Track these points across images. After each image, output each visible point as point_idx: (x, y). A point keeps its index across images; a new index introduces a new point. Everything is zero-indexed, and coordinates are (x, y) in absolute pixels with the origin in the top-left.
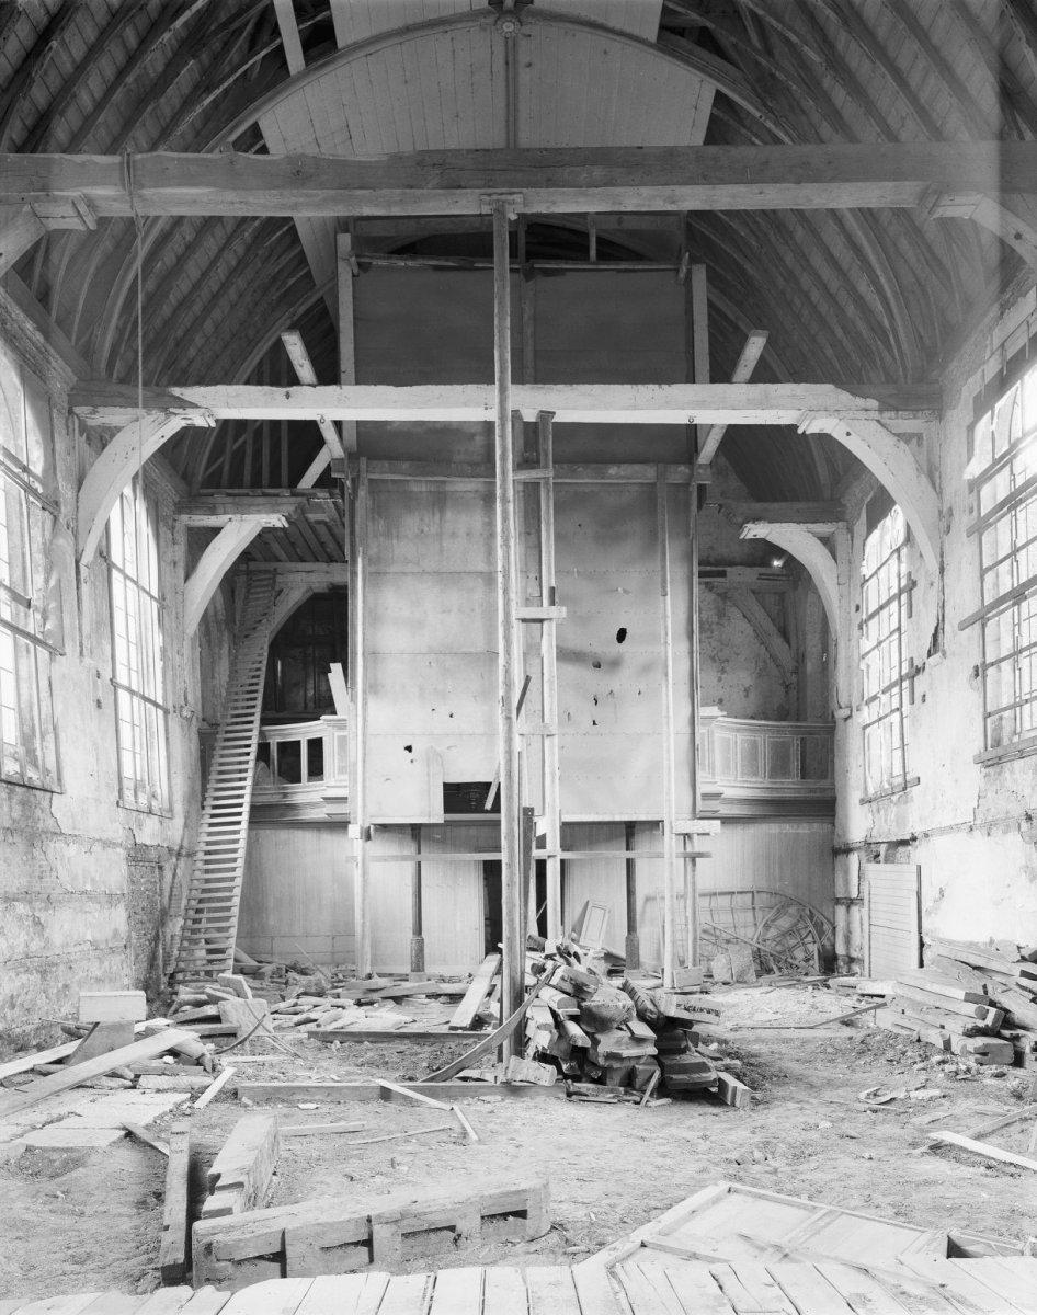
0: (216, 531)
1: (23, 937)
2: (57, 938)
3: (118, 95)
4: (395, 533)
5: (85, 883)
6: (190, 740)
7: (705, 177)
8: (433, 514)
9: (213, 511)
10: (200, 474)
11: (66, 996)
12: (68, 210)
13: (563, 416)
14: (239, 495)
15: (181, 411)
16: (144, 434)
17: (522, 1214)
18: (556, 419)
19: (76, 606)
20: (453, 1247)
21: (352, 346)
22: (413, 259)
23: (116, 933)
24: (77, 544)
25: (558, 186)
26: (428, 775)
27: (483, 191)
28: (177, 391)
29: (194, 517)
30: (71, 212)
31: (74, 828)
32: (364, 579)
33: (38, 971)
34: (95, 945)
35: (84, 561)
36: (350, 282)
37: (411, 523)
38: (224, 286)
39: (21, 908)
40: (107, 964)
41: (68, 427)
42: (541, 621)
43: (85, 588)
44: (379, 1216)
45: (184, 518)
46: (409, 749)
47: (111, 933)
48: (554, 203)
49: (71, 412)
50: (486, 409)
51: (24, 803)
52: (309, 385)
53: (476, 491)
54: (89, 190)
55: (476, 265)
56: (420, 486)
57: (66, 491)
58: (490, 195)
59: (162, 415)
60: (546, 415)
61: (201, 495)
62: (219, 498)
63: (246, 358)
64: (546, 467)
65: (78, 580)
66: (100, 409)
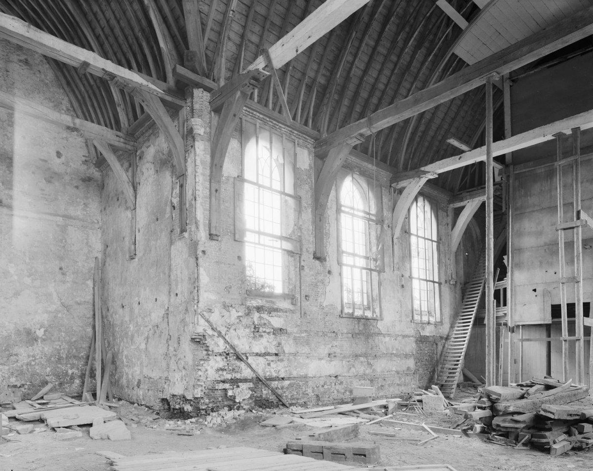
0: (463, 207)
1: (362, 368)
2: (379, 370)
3: (393, 78)
4: (529, 193)
5: (392, 351)
6: (455, 293)
7: (576, 27)
8: (547, 181)
9: (462, 200)
10: (447, 193)
11: (382, 389)
12: (355, 140)
13: (584, 127)
14: (471, 191)
15: (424, 175)
16: (414, 186)
17: (365, 456)
18: (582, 129)
19: (392, 254)
20: (344, 460)
21: (510, 117)
22: (536, 69)
23: (408, 369)
24: (392, 232)
25: (509, 63)
26: (544, 302)
27: (480, 77)
28: (422, 169)
29: (455, 204)
30: (356, 140)
31: (388, 331)
32: (512, 219)
33: (369, 380)
34: (398, 373)
35: (395, 237)
36: (509, 90)
37: (537, 188)
38: (457, 114)
39: (362, 359)
40: (403, 379)
41: (389, 192)
42: (573, 228)
43: (396, 247)
44: (325, 447)
45: (451, 206)
46: (535, 290)
47: (406, 369)
48: (511, 68)
49: (391, 186)
50: (544, 136)
51: (364, 325)
52: (469, 151)
53: (569, 165)
54: (359, 132)
55: (568, 58)
56: (541, 170)
57: (387, 213)
58: (482, 78)
59: (418, 179)
60: (576, 130)
61: (457, 195)
62: (464, 194)
63: (475, 134)
64: (576, 153)
65: (393, 244)
66: (399, 183)
